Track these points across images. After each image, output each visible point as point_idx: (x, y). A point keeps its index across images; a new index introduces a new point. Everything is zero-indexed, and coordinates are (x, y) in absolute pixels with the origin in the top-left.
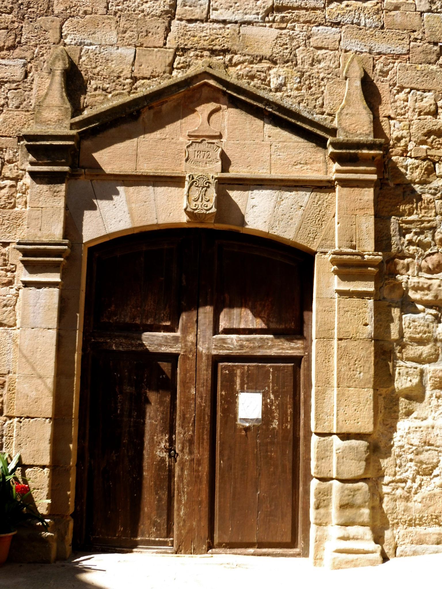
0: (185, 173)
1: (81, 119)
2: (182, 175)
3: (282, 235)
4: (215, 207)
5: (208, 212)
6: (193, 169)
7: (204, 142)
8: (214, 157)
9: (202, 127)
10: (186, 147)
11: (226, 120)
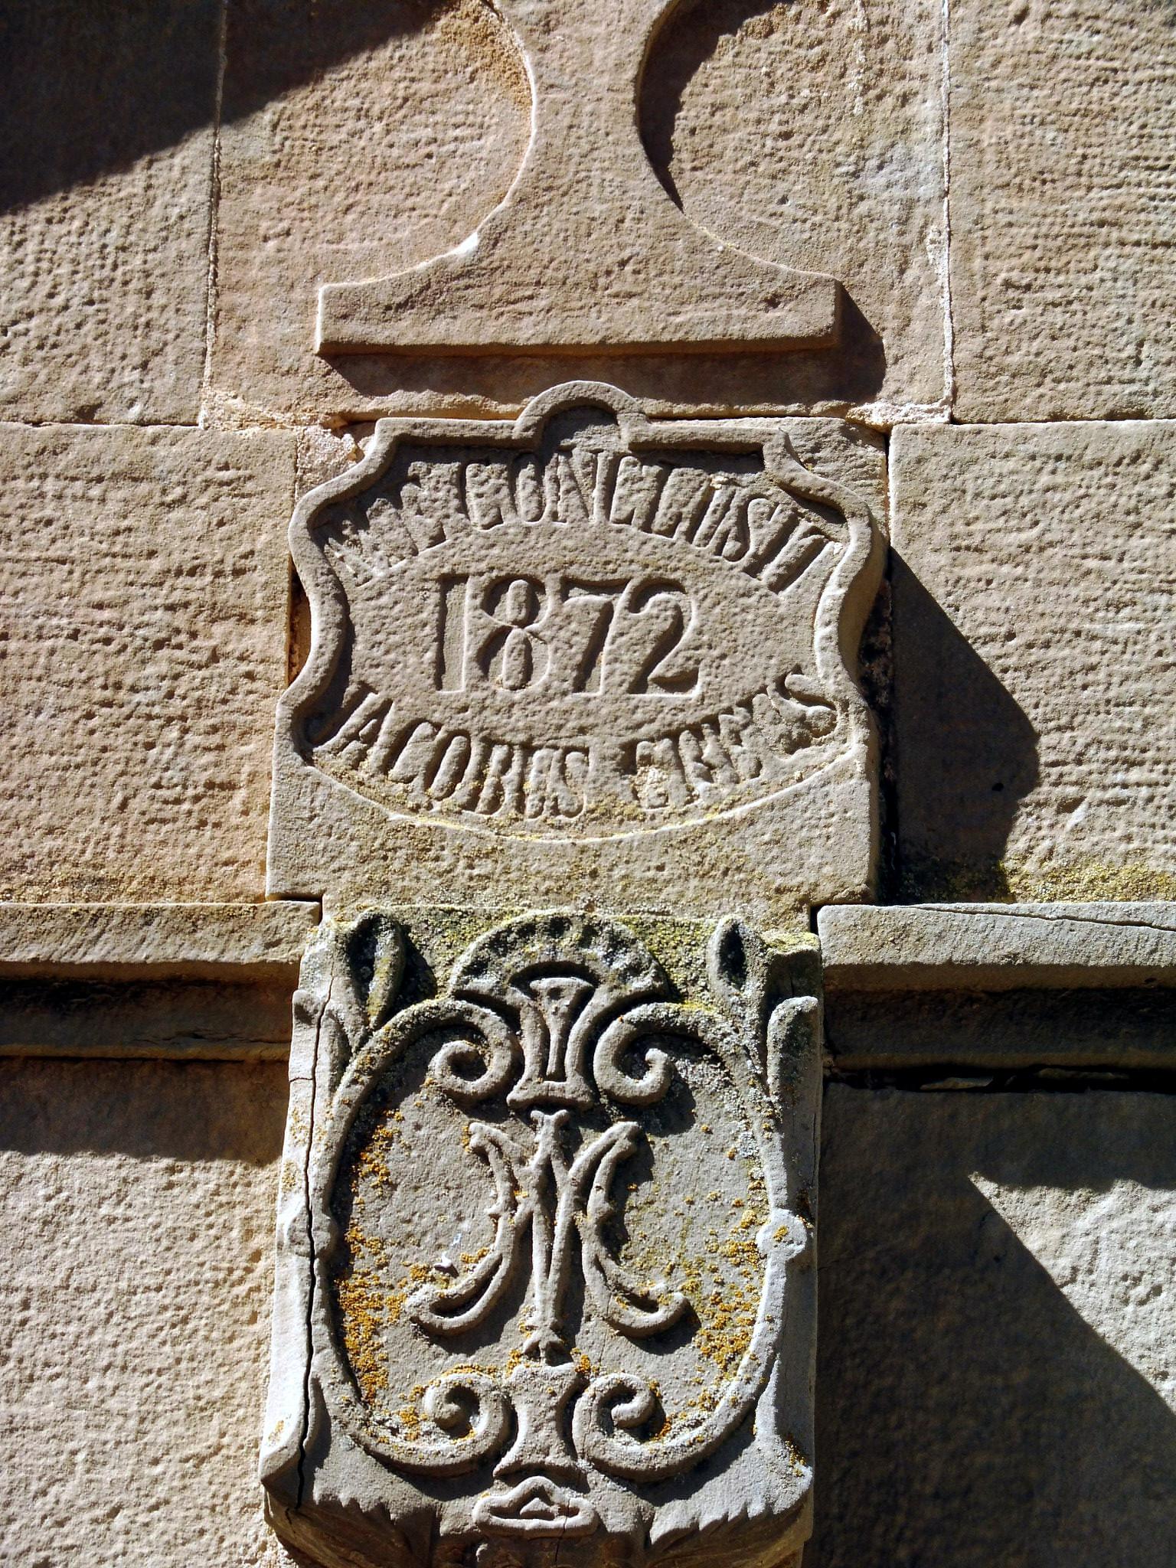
0: (289, 918)
1: (377, 399)
2: (248, 952)
3: (864, 839)
4: (785, 1430)
5: (668, 1519)
6: (424, 847)
7: (583, 441)
8: (754, 672)
9: (554, 219)
10: (297, 521)
11: (927, 109)
